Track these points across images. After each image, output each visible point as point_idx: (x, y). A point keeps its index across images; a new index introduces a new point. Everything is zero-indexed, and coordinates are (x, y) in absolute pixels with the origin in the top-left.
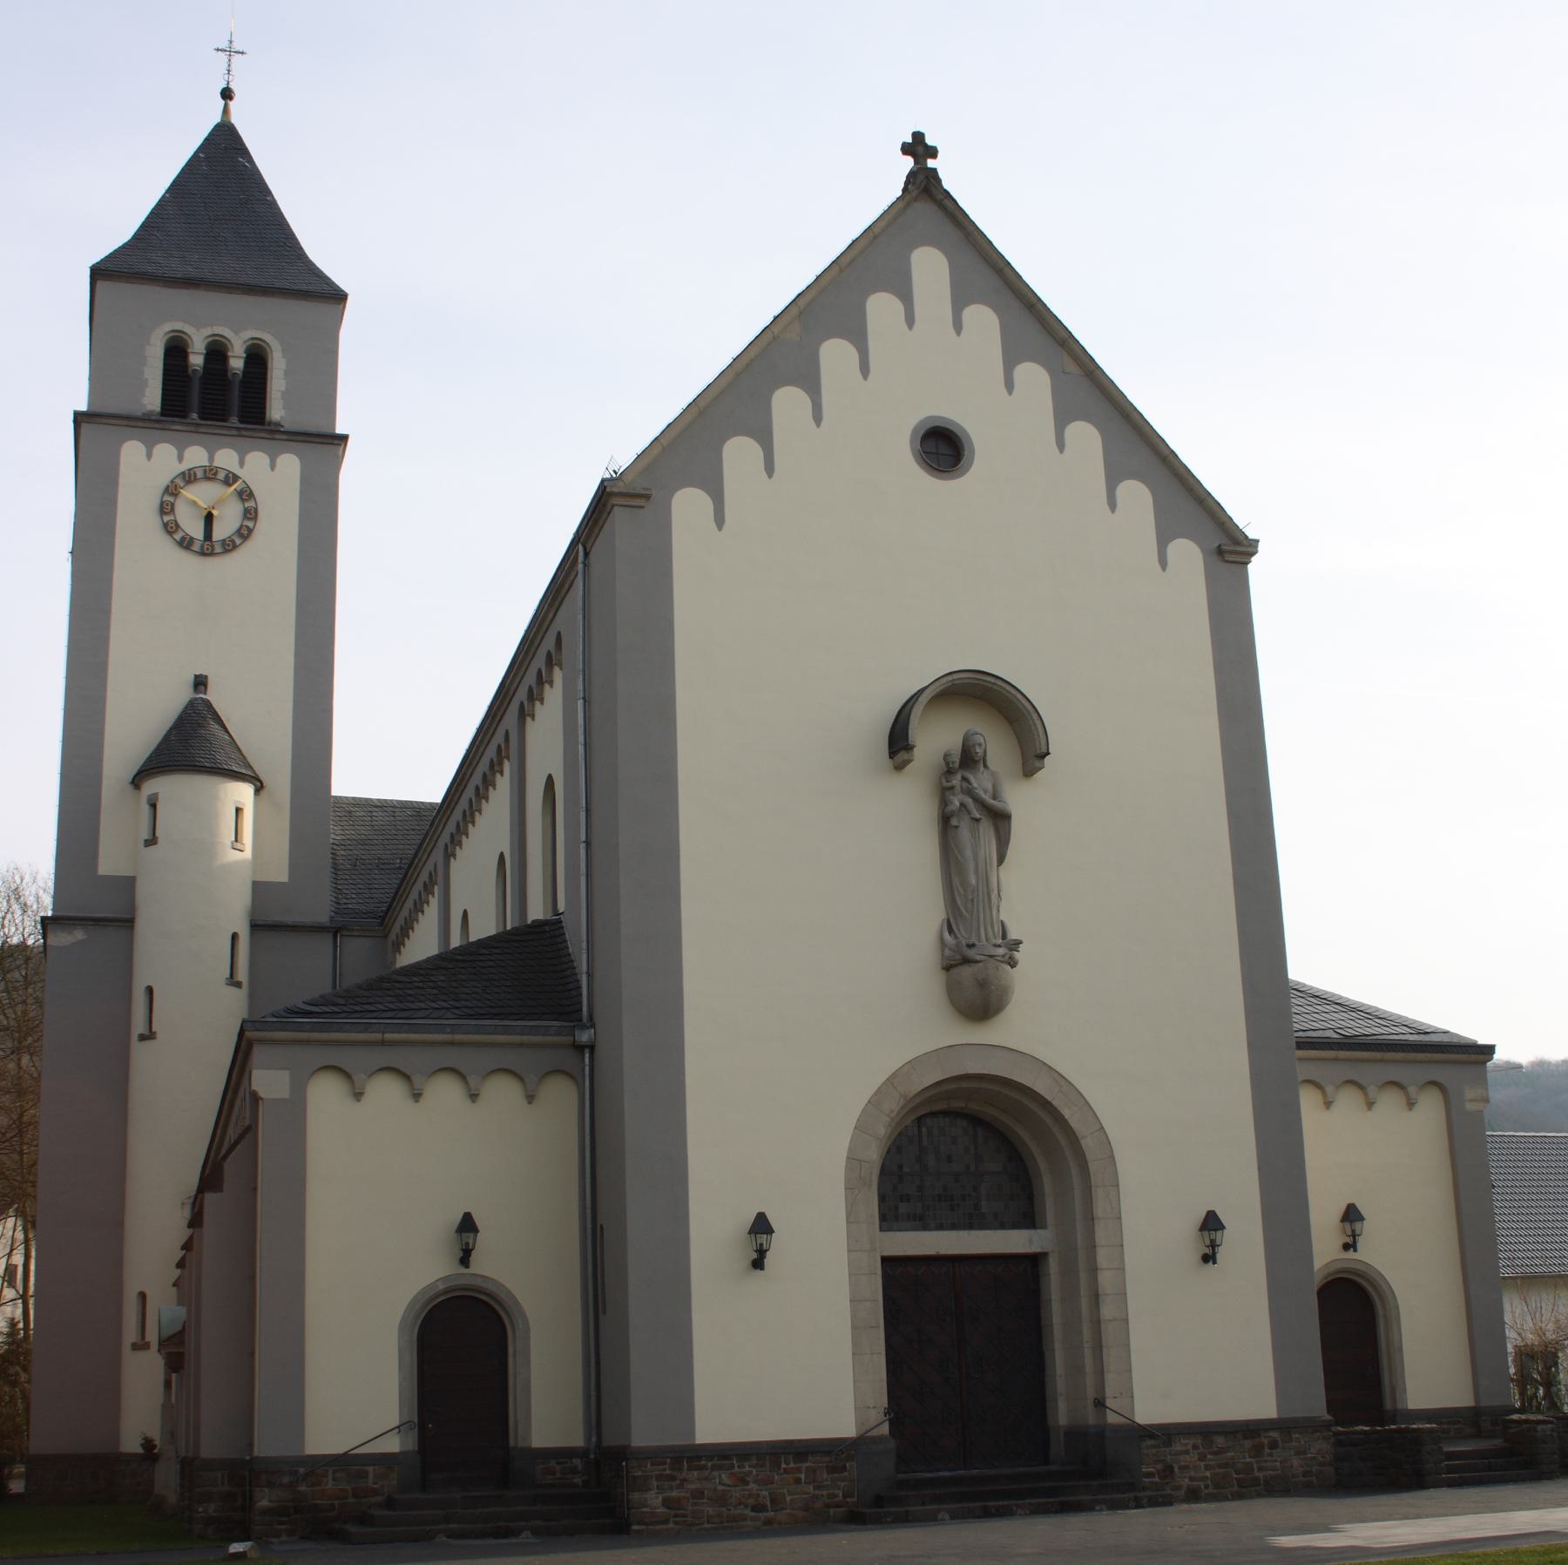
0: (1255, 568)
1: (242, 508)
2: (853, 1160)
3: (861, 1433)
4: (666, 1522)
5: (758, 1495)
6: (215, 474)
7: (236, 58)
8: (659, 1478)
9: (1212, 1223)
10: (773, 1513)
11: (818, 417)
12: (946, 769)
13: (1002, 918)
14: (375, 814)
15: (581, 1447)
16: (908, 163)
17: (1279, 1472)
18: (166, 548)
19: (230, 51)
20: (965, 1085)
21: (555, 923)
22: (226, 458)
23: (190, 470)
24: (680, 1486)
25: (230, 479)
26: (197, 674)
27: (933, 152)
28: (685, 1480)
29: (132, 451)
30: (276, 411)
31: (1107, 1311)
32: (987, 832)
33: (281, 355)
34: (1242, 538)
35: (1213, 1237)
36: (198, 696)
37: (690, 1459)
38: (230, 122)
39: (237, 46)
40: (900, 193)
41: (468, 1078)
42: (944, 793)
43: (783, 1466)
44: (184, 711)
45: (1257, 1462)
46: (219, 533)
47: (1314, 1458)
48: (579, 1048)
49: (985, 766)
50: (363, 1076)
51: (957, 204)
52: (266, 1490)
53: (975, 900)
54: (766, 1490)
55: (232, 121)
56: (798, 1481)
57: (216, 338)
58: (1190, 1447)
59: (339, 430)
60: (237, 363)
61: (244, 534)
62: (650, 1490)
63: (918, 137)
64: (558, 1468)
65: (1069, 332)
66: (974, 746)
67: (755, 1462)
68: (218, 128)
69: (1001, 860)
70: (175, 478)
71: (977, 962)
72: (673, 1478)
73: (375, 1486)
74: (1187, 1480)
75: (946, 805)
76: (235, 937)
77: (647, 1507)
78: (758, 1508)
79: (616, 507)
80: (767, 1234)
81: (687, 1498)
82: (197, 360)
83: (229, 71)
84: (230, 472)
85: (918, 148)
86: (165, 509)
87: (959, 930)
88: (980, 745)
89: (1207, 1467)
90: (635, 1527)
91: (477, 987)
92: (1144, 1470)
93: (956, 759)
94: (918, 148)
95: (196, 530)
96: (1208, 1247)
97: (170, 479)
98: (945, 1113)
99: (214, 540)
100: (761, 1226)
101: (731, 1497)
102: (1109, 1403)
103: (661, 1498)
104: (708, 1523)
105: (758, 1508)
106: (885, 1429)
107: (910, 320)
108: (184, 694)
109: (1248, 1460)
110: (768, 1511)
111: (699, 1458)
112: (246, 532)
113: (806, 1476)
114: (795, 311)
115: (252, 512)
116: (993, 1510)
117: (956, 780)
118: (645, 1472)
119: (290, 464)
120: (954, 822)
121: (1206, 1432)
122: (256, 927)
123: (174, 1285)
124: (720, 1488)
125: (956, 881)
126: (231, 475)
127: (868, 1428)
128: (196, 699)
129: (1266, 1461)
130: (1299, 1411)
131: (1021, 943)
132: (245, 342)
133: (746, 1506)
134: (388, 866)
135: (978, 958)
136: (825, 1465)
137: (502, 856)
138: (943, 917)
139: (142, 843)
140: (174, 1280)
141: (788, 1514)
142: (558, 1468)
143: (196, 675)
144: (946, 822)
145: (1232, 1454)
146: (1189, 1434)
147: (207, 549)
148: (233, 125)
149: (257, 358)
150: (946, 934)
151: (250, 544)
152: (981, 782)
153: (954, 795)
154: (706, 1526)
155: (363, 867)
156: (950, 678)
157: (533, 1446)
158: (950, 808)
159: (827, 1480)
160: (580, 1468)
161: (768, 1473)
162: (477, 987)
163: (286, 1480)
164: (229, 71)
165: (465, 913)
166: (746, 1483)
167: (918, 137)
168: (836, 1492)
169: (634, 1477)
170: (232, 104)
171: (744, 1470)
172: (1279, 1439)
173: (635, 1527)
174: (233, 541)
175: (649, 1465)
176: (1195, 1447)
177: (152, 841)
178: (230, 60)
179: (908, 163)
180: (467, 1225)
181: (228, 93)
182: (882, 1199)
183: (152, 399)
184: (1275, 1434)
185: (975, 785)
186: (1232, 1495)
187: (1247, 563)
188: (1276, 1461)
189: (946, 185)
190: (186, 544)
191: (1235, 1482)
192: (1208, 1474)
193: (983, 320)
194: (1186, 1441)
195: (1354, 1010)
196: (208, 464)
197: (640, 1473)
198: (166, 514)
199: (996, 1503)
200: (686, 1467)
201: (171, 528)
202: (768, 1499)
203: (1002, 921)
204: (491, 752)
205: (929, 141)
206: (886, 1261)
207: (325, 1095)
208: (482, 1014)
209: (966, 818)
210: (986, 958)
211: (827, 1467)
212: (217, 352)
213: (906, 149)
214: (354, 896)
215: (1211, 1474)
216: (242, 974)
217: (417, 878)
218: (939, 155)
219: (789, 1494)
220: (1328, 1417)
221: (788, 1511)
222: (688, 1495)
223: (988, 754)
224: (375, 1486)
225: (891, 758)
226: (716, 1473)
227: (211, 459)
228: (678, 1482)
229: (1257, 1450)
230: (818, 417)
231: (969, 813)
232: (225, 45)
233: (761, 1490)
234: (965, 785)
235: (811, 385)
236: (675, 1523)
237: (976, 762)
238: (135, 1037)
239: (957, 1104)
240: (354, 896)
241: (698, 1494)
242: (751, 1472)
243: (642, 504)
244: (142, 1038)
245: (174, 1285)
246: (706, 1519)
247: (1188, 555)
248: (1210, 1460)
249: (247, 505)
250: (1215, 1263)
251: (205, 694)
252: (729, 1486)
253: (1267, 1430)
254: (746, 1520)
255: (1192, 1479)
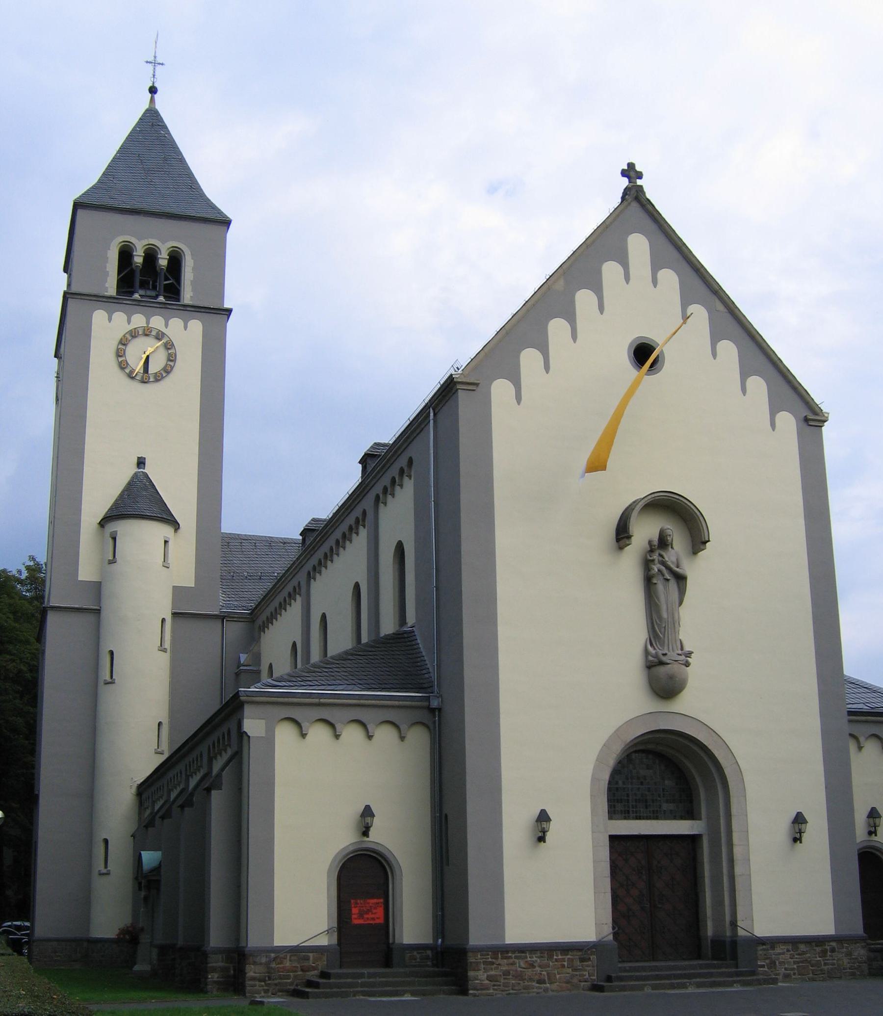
0: (826, 429)
1: (167, 354)
2: (594, 780)
3: (600, 937)
4: (488, 989)
5: (541, 974)
6: (151, 332)
7: (158, 68)
8: (485, 963)
9: (799, 820)
10: (548, 985)
11: (574, 337)
12: (649, 549)
13: (680, 638)
14: (244, 544)
15: (431, 944)
16: (625, 182)
17: (836, 966)
18: (120, 377)
19: (155, 63)
20: (658, 736)
21: (410, 633)
22: (157, 322)
23: (135, 329)
24: (497, 968)
25: (159, 336)
26: (140, 456)
27: (640, 176)
28: (499, 964)
29: (99, 317)
30: (187, 295)
31: (738, 870)
32: (673, 584)
33: (190, 258)
34: (819, 411)
35: (800, 827)
36: (140, 470)
37: (502, 952)
38: (155, 108)
39: (159, 60)
40: (620, 201)
41: (368, 726)
42: (647, 564)
43: (555, 957)
44: (133, 477)
45: (823, 960)
46: (153, 369)
47: (856, 958)
48: (432, 711)
49: (672, 548)
50: (308, 724)
51: (655, 208)
52: (252, 966)
53: (667, 627)
54: (545, 971)
55: (157, 107)
56: (563, 966)
57: (150, 246)
58: (785, 950)
59: (227, 305)
60: (163, 262)
61: (167, 370)
62: (480, 970)
63: (631, 166)
64: (418, 956)
65: (720, 286)
66: (667, 536)
67: (539, 955)
68: (147, 111)
69: (681, 603)
70: (125, 334)
71: (668, 664)
72: (493, 963)
73: (313, 965)
74: (783, 970)
75: (649, 571)
76: (163, 620)
77: (477, 980)
78: (541, 982)
79: (459, 390)
80: (546, 821)
81: (501, 975)
82: (138, 259)
83: (154, 75)
84: (160, 331)
85: (631, 172)
86: (119, 354)
87: (657, 646)
88: (670, 535)
89: (795, 963)
90: (471, 992)
91: (370, 671)
92: (759, 963)
93: (656, 542)
94: (631, 172)
95: (139, 367)
96: (797, 833)
97: (123, 335)
98: (643, 751)
99: (149, 373)
100: (543, 817)
101: (526, 974)
102: (739, 923)
103: (486, 975)
104: (512, 989)
105: (541, 982)
106: (611, 937)
107: (627, 278)
108: (130, 470)
109: (819, 959)
110: (546, 984)
111: (507, 952)
112: (169, 368)
113: (567, 964)
114: (560, 271)
115: (173, 356)
116: (676, 985)
117: (655, 557)
118: (476, 959)
119: (196, 326)
120: (655, 581)
121: (794, 942)
122: (175, 615)
123: (132, 836)
124: (519, 969)
125: (655, 616)
126: (160, 332)
127: (603, 936)
128: (139, 472)
129: (828, 960)
130: (846, 932)
131: (693, 653)
132: (168, 249)
133: (534, 981)
134: (253, 578)
135: (668, 661)
136: (577, 957)
137: (357, 586)
138: (647, 637)
139: (107, 562)
140: (132, 833)
141: (557, 985)
142: (418, 956)
143: (138, 458)
144: (648, 581)
145: (810, 955)
146: (785, 942)
147: (146, 379)
148: (157, 110)
149: (176, 260)
150: (649, 647)
151: (171, 375)
152: (670, 556)
153: (654, 565)
154: (511, 991)
155: (238, 578)
156: (653, 496)
157: (404, 943)
158: (652, 572)
159: (579, 966)
160: (430, 955)
161: (546, 961)
162: (370, 671)
163: (264, 960)
164: (154, 75)
165: (324, 617)
166: (534, 967)
167: (631, 166)
168: (585, 973)
169: (471, 962)
170: (156, 96)
171: (533, 959)
172: (836, 947)
173: (471, 992)
174: (161, 374)
175: (479, 956)
176: (788, 951)
177: (113, 561)
178: (154, 69)
179: (625, 182)
180: (368, 812)
181: (153, 89)
182: (609, 801)
183: (111, 287)
184: (834, 944)
185: (667, 559)
186: (809, 979)
187: (822, 426)
188: (834, 959)
189: (648, 196)
190: (131, 376)
191: (811, 972)
192: (795, 966)
193: (669, 278)
194: (783, 947)
195: (875, 692)
196: (146, 326)
197: (474, 960)
198: (121, 356)
199: (677, 981)
200: (500, 957)
201: (123, 366)
202: (546, 976)
203: (680, 640)
204: (350, 520)
205: (638, 168)
206: (612, 838)
207: (285, 734)
208: (375, 688)
209: (661, 578)
210: (673, 661)
211: (579, 958)
212: (151, 255)
213: (624, 173)
214: (233, 596)
215: (797, 966)
216: (167, 645)
217: (282, 590)
218: (644, 177)
219: (559, 974)
220: (865, 935)
221: (558, 984)
222: (501, 973)
223: (674, 541)
224: (313, 965)
225: (617, 541)
226: (517, 961)
227: (148, 322)
228: (495, 966)
229: (824, 952)
230: (574, 337)
231: (663, 575)
232: (151, 59)
233: (543, 971)
234: (661, 559)
235: (571, 318)
236: (494, 989)
237: (667, 545)
238: (101, 683)
239: (650, 747)
240: (233, 596)
241: (506, 973)
242: (536, 961)
243: (474, 389)
244: (107, 683)
245: (132, 836)
246: (511, 988)
247: (787, 421)
248: (796, 958)
249: (170, 352)
250: (801, 842)
251: (144, 469)
252: (524, 968)
253: (829, 942)
254: (533, 989)
255: (786, 969)
